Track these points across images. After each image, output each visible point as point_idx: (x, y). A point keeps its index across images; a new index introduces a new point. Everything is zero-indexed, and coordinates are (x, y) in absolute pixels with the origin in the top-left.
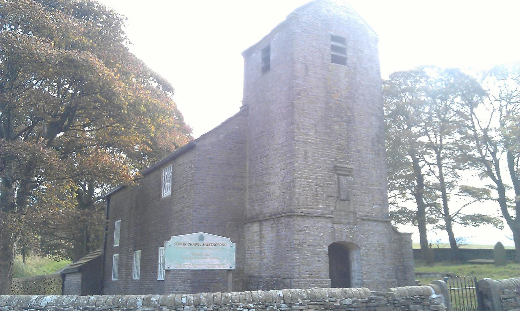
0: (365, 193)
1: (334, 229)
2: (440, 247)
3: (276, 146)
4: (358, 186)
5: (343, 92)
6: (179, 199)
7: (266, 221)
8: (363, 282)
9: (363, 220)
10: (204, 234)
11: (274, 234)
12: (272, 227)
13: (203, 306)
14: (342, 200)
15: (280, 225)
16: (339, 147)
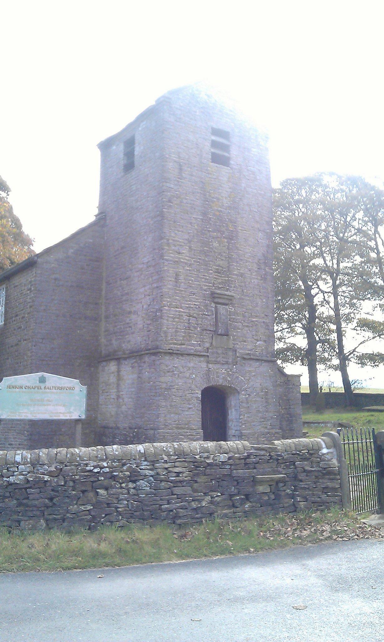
1: (209, 370)
3: (140, 266)
5: (225, 201)
7: (125, 359)
8: (241, 433)
9: (244, 359)
11: (135, 376)
12: (133, 367)
13: (43, 465)
14: (221, 335)
15: (142, 364)
16: (217, 269)
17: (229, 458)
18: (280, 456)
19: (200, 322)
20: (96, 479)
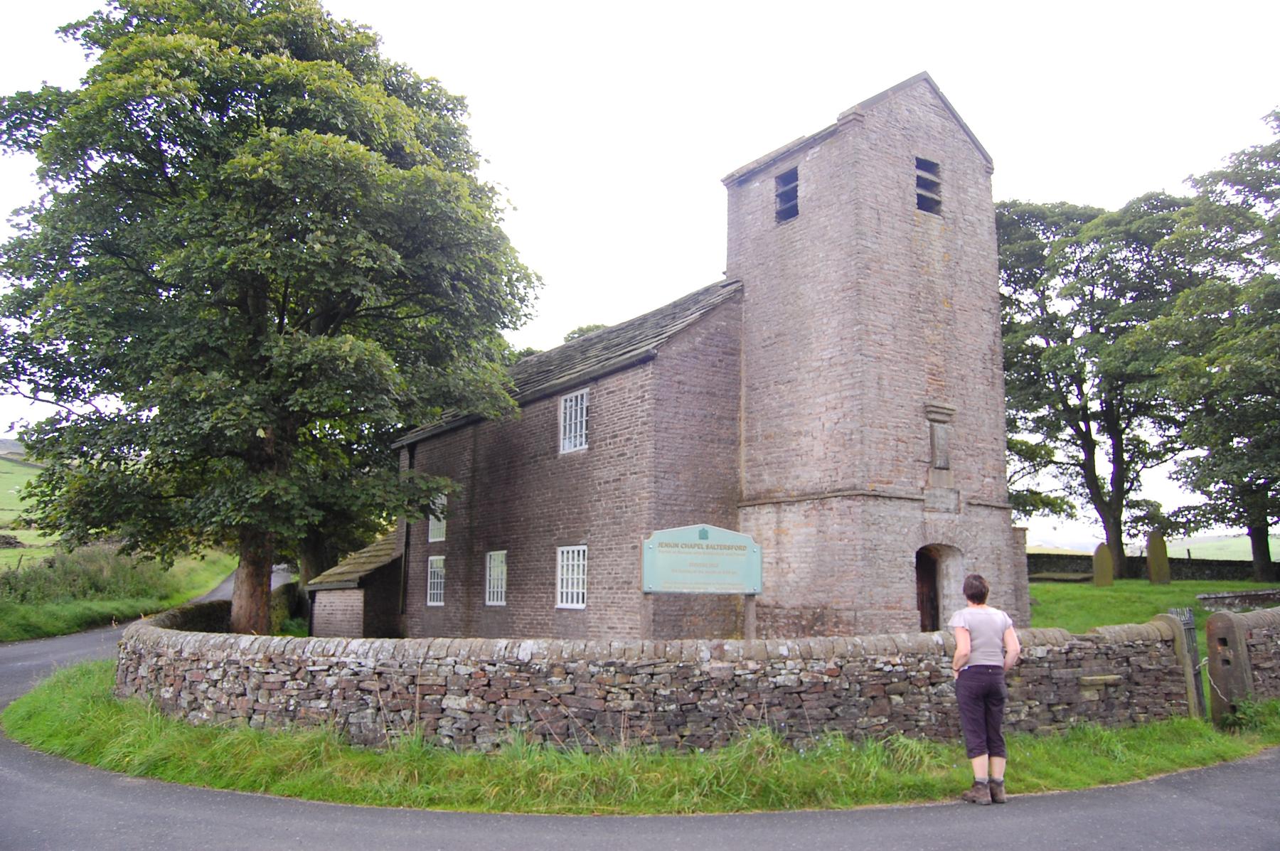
0: (971, 456)
1: (924, 523)
2: (1193, 556)
3: (816, 364)
4: (962, 442)
5: (937, 266)
6: (611, 458)
7: (791, 503)
9: (970, 504)
10: (708, 527)
11: (813, 530)
12: (806, 517)
13: (818, 659)
14: (940, 468)
15: (827, 512)
17: (1048, 652)
18: (1110, 648)
19: (911, 450)
20: (888, 681)
